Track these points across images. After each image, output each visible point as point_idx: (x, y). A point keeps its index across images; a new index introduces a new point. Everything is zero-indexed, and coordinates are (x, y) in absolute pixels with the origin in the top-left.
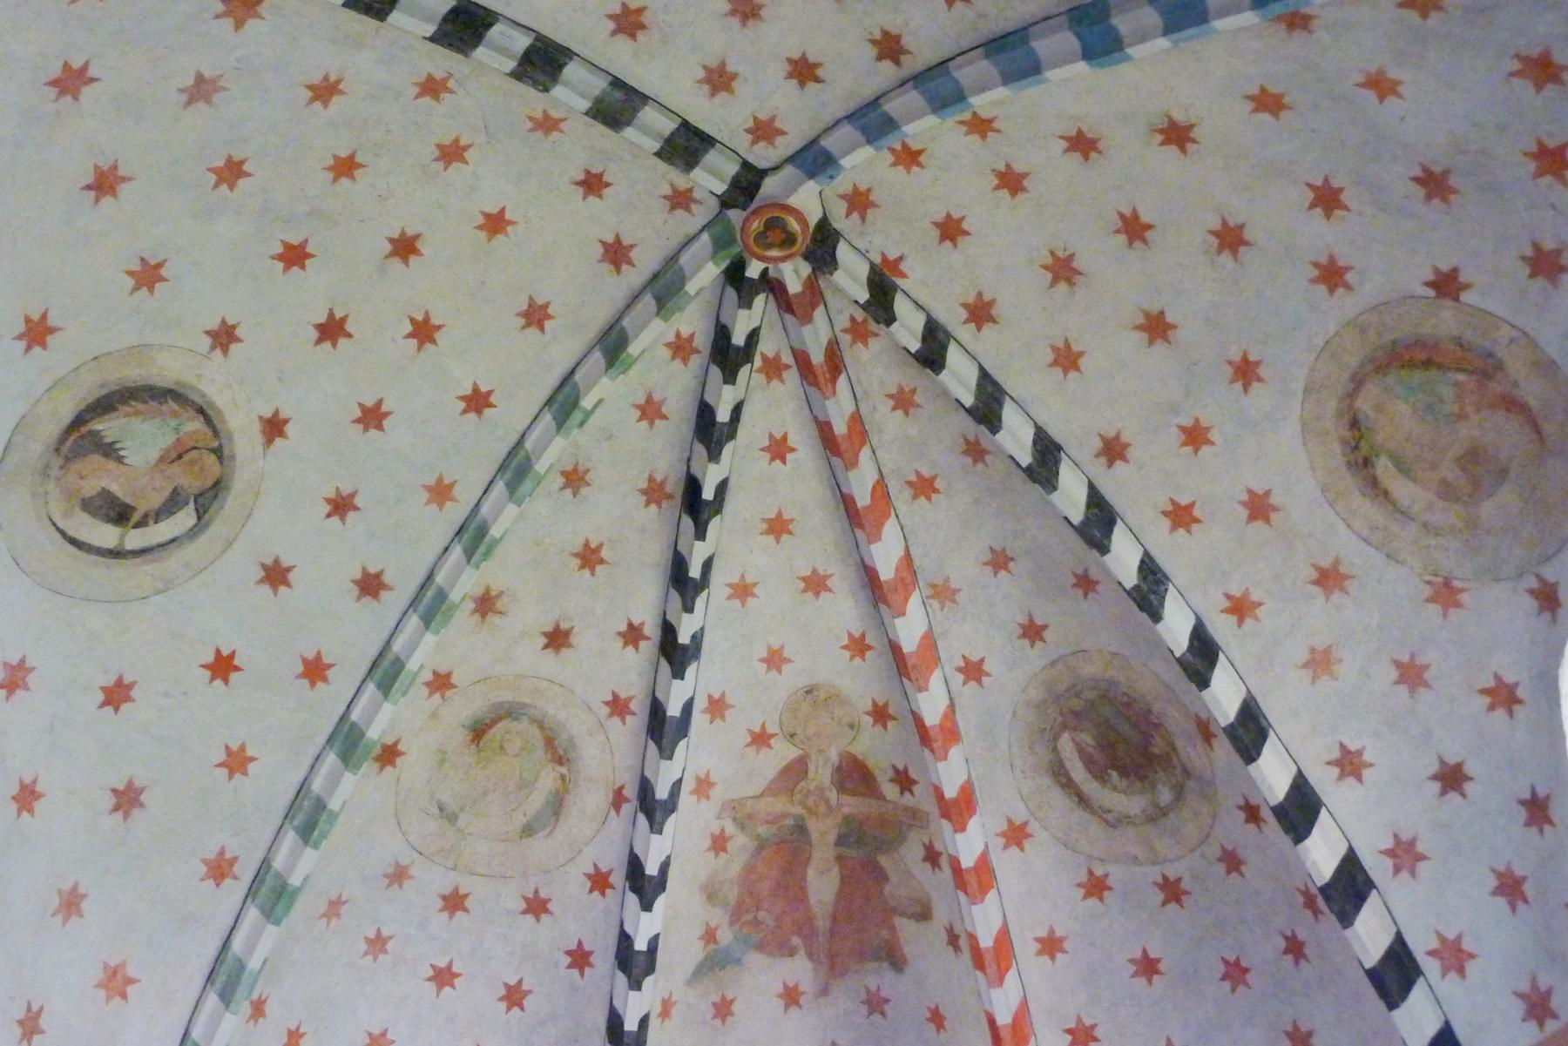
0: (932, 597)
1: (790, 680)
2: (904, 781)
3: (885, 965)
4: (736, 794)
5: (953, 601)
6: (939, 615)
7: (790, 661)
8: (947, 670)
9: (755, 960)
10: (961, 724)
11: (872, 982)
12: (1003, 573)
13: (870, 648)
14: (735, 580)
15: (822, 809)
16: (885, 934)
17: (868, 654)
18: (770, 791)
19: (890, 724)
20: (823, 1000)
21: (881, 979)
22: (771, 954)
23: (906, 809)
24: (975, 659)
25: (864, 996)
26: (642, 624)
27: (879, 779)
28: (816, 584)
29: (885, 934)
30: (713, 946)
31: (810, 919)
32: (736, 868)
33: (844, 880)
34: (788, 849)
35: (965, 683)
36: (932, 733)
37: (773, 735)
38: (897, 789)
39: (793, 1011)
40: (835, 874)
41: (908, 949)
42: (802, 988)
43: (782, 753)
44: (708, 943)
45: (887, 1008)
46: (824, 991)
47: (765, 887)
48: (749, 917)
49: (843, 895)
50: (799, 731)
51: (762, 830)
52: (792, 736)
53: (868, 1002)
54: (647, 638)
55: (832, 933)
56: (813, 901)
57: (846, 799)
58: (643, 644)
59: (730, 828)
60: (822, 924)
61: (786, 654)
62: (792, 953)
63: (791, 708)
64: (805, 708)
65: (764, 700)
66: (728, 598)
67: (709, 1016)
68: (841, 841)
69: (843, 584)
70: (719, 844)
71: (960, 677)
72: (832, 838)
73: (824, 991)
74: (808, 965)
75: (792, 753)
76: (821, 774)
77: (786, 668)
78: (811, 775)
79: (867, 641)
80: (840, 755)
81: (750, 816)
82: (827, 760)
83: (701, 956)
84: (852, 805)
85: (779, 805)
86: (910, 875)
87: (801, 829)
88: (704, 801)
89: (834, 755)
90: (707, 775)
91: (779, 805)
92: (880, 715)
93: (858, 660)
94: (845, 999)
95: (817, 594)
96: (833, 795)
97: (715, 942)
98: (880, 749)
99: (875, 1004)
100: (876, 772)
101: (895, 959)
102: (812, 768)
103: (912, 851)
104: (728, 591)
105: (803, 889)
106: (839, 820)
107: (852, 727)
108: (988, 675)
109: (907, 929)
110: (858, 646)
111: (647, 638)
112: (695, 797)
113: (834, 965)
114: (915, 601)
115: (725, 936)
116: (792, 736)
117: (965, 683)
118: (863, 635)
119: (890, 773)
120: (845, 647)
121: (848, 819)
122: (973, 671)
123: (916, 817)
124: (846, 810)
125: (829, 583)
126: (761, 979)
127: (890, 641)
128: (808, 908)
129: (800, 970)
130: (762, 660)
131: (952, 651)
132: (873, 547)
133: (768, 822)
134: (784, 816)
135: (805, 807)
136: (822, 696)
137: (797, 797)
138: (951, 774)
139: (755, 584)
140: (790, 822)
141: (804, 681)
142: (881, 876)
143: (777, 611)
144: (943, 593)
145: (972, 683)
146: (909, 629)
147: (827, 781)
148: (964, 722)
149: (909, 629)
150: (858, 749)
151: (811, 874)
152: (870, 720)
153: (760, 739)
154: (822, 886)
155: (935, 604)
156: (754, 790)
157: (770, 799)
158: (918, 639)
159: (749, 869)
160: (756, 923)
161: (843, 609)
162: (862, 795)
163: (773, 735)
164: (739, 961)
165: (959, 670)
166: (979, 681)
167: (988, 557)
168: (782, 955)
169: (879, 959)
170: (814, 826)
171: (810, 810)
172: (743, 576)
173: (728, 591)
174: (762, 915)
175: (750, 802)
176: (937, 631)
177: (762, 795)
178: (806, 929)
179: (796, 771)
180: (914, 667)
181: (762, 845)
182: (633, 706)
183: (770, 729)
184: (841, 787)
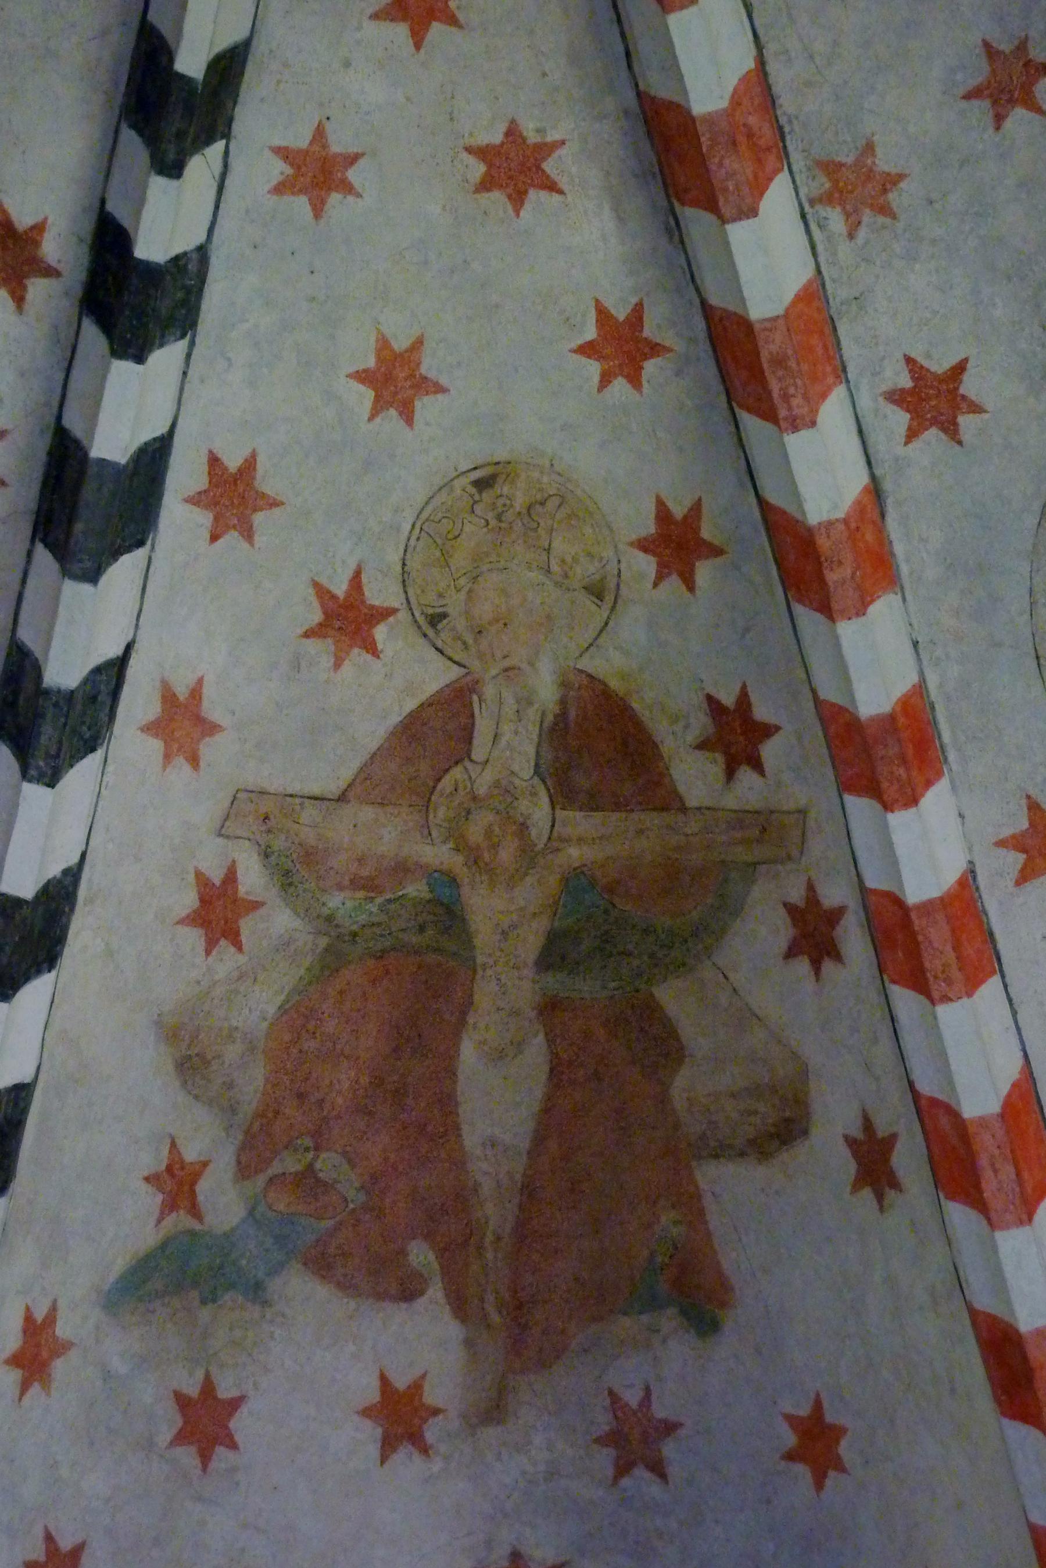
0: (827, 199)
1: (435, 445)
2: (736, 735)
3: (669, 1320)
4: (275, 776)
5: (885, 210)
6: (845, 250)
7: (440, 389)
8: (865, 402)
9: (300, 1290)
10: (899, 549)
11: (628, 1378)
12: (1019, 115)
13: (655, 349)
14: (300, 138)
15: (507, 854)
16: (668, 1222)
17: (651, 367)
18: (367, 786)
19: (704, 571)
20: (490, 1433)
21: (664, 1367)
22: (347, 1287)
23: (740, 819)
24: (940, 364)
25: (604, 1423)
26: (39, 228)
27: (668, 745)
28: (514, 169)
29: (668, 1222)
30: (181, 1220)
31: (462, 1197)
32: (261, 1005)
33: (558, 1072)
34: (406, 968)
35: (912, 435)
36: (823, 543)
37: (385, 613)
38: (713, 766)
39: (404, 1457)
40: (536, 1052)
41: (738, 1255)
42: (431, 1396)
43: (403, 672)
44: (170, 1206)
45: (669, 1450)
46: (492, 1410)
47: (341, 1082)
48: (290, 1164)
49: (550, 1123)
50: (455, 603)
51: (339, 902)
52: (435, 620)
53: (614, 1438)
54: (50, 272)
55: (523, 1234)
56: (471, 1139)
57: (578, 822)
58: (37, 288)
59: (253, 878)
60: (495, 1213)
61: (429, 367)
62: (408, 1292)
63: (435, 533)
64: (473, 533)
65: (357, 498)
66: (279, 189)
67: (165, 1435)
68: (554, 955)
69: (589, 154)
70: (218, 912)
71: (900, 419)
72: (531, 941)
73: (492, 1410)
74: (453, 1330)
75: (434, 676)
76: (509, 746)
77: (426, 407)
78: (479, 753)
79: (649, 331)
80: (565, 685)
81: (310, 856)
82: (526, 701)
83: (148, 1237)
84: (590, 839)
85: (384, 833)
86: (746, 1017)
87: (446, 914)
88: (181, 766)
89: (546, 691)
90: (196, 692)
91: (384, 833)
92: (677, 544)
93: (620, 386)
94: (547, 1441)
95: (518, 199)
96: (538, 811)
97: (194, 1210)
98: (666, 651)
99: (636, 1442)
100: (660, 729)
101: (696, 1295)
102: (483, 727)
103: (761, 929)
104: (279, 169)
105: (447, 1103)
106: (553, 880)
107: (596, 591)
108: (976, 409)
109: (729, 1186)
110: (622, 347)
111: (50, 272)
112: (156, 745)
113: (523, 1329)
114: (778, 199)
115: (223, 1202)
116: (435, 620)
117: (912, 435)
118: (638, 313)
119: (700, 723)
120: (587, 350)
121: (577, 882)
122: (934, 400)
123: (771, 833)
124: (574, 854)
125: (549, 166)
126: (319, 1358)
127: (707, 309)
128: (459, 1162)
129: (425, 1342)
130: (363, 377)
131: (879, 343)
132: (675, 21)
133: (356, 883)
134: (402, 869)
135: (461, 845)
136: (520, 501)
137: (441, 814)
138: (875, 658)
139: (353, 159)
140: (416, 889)
141: (471, 451)
142: (663, 1047)
143: (408, 244)
144: (856, 188)
145: (933, 435)
146: (767, 257)
147: (524, 769)
148: (913, 540)
149: (767, 257)
150: (608, 664)
151: (468, 1052)
152: (646, 564)
153: (347, 620)
154: (497, 1096)
155: (835, 219)
156: (328, 775)
157: (367, 813)
158: (789, 297)
159: (298, 1018)
160: (308, 1183)
161: (586, 241)
162: (618, 805)
163: (385, 613)
164: (256, 1291)
165: (897, 397)
166: (951, 429)
167: (978, 72)
168: (381, 1296)
169: (653, 1303)
170: (485, 908)
171: (474, 858)
172: (319, 134)
173: (279, 169)
174: (328, 1164)
175: (310, 813)
176: (838, 293)
177: (342, 798)
178: (449, 1218)
179: (440, 731)
180: (779, 361)
181: (331, 962)
182: (51, 249)
183: (380, 592)
184: (564, 792)
